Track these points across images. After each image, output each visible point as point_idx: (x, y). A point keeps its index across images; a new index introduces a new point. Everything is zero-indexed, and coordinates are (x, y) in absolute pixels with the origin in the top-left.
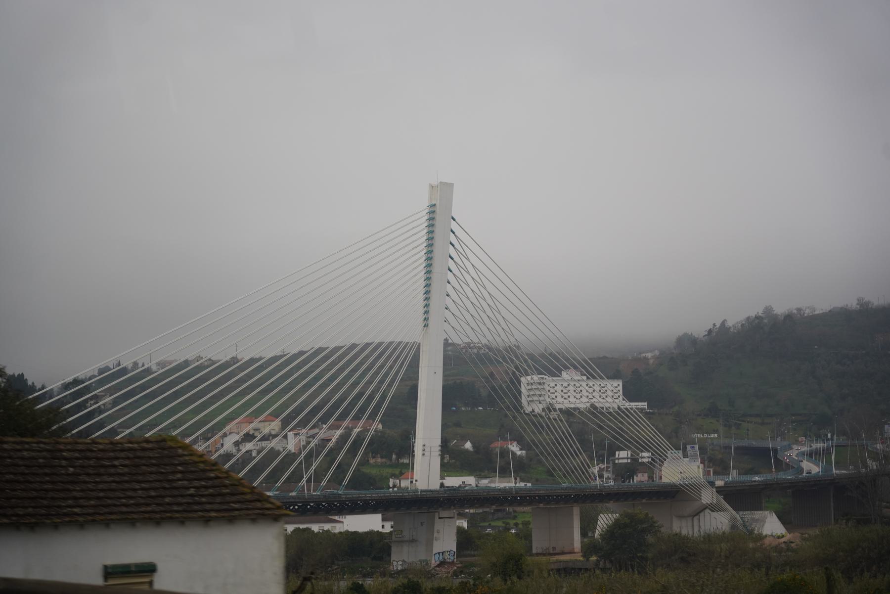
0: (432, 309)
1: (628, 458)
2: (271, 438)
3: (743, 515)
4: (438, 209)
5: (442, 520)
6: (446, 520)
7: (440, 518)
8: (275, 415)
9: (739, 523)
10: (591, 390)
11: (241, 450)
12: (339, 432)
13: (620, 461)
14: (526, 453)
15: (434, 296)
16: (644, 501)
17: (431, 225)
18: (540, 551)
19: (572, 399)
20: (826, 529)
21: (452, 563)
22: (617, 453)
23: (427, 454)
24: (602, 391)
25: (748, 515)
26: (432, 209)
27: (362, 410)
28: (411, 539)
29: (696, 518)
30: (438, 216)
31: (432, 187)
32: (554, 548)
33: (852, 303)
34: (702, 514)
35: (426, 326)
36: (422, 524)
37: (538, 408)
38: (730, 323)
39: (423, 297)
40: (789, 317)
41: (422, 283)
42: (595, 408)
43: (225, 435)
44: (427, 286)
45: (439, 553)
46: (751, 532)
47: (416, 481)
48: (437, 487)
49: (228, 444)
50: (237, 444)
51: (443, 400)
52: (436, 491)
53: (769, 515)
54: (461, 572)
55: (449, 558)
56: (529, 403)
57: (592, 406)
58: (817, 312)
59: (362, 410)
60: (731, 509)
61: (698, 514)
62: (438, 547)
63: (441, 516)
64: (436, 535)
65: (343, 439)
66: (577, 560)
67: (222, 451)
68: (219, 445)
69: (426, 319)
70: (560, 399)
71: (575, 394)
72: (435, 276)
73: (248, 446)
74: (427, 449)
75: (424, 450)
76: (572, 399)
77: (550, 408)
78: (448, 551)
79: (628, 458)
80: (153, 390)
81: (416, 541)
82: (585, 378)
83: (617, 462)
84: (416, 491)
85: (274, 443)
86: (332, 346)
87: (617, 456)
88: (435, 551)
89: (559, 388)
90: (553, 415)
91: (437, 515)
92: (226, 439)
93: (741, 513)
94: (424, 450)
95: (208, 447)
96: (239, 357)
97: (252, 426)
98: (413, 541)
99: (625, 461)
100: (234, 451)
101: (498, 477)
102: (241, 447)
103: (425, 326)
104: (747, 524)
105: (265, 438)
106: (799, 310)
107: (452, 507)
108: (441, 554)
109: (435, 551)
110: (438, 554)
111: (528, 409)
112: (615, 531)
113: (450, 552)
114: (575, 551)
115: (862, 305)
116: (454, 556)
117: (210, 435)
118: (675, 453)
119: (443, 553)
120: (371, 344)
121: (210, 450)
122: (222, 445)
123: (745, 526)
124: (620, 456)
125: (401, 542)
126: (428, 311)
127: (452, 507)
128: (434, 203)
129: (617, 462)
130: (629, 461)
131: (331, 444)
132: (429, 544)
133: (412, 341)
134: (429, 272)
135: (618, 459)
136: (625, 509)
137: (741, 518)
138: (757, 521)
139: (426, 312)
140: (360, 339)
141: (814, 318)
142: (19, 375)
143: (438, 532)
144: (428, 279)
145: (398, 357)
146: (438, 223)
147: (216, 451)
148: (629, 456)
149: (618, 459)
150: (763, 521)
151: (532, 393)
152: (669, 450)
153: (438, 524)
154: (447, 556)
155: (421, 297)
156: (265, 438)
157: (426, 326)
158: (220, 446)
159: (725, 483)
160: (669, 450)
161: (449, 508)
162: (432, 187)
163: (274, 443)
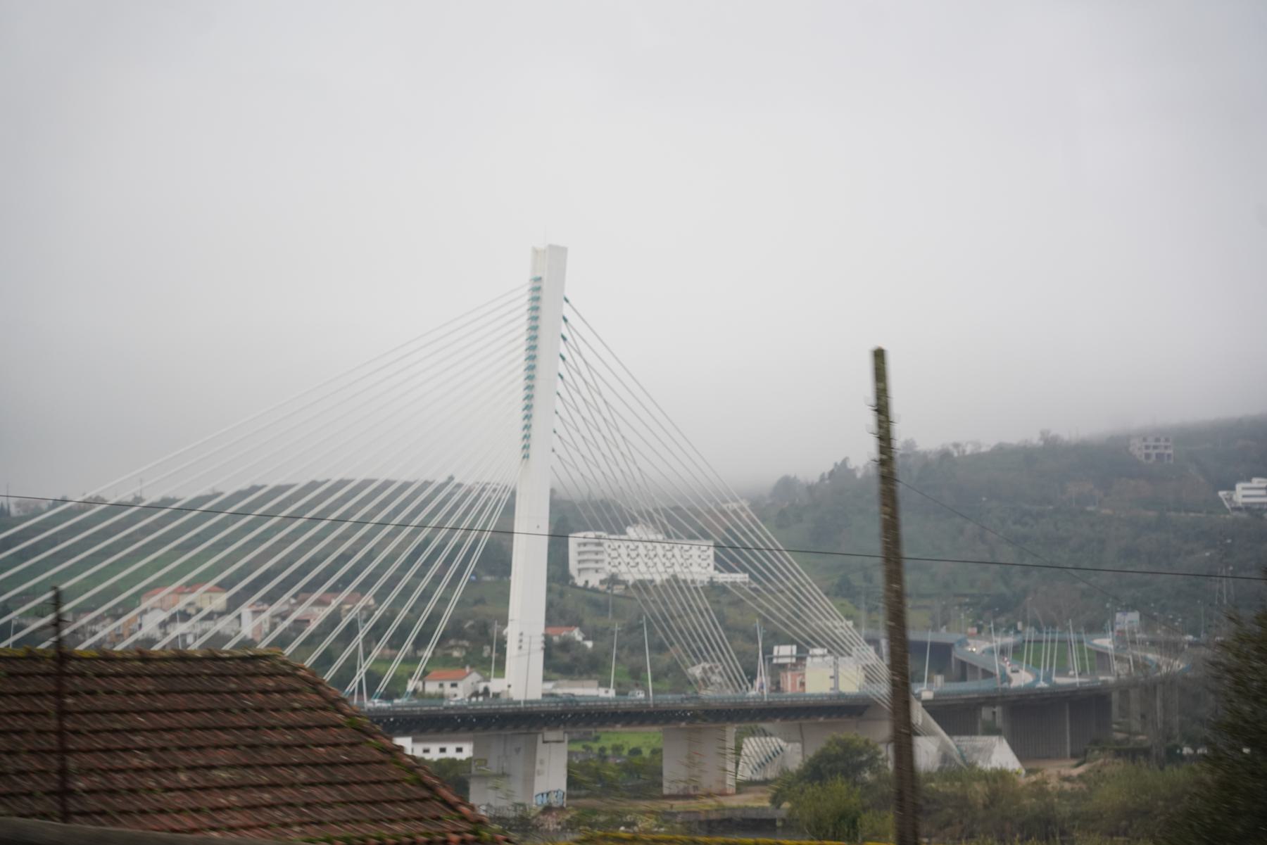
0: (534, 432)
1: (791, 656)
2: (215, 616)
3: (959, 741)
4: (545, 285)
5: (548, 745)
6: (554, 745)
7: (545, 742)
8: (224, 586)
9: (955, 753)
10: (633, 554)
11: (168, 634)
12: (328, 610)
13: (781, 661)
14: (594, 646)
15: (537, 413)
16: (821, 719)
17: (535, 309)
18: (674, 791)
19: (695, 568)
21: (562, 808)
22: (776, 648)
23: (525, 646)
24: (703, 557)
25: (966, 741)
26: (537, 285)
27: (345, 581)
28: (500, 772)
30: (545, 295)
33: (1035, 439)
35: (526, 457)
36: (518, 750)
37: (594, 580)
38: (852, 464)
39: (523, 414)
40: (945, 455)
41: (521, 393)
42: (677, 581)
43: (145, 612)
44: (529, 397)
45: (542, 794)
46: (972, 766)
49: (150, 626)
50: (163, 625)
51: (549, 564)
52: (537, 702)
53: (997, 742)
54: (579, 823)
55: (555, 801)
56: (580, 570)
57: (675, 577)
58: (984, 449)
59: (345, 581)
60: (938, 729)
62: (541, 785)
63: (546, 739)
64: (538, 767)
65: (333, 620)
66: (746, 807)
67: (139, 635)
68: (135, 626)
69: (526, 447)
70: (623, 568)
71: (699, 561)
72: (540, 384)
73: (179, 629)
74: (526, 639)
75: (521, 641)
76: (642, 568)
77: (613, 580)
78: (554, 792)
79: (791, 656)
80: (163, 547)
81: (508, 776)
82: (660, 537)
85: (222, 625)
86: (272, 484)
87: (775, 653)
88: (536, 792)
89: (623, 551)
90: (618, 589)
91: (540, 738)
92: (147, 618)
93: (956, 738)
94: (521, 641)
96: (144, 496)
97: (190, 598)
98: (504, 775)
100: (158, 634)
101: (495, 670)
102: (169, 629)
103: (524, 457)
104: (965, 755)
105: (210, 617)
106: (956, 446)
107: (562, 726)
108: (545, 796)
109: (536, 792)
110: (541, 796)
111: (580, 582)
112: (822, 766)
113: (557, 792)
114: (728, 792)
115: (1046, 441)
116: (563, 798)
117: (120, 611)
118: (863, 650)
119: (548, 794)
120: (348, 482)
121: (121, 632)
122: (140, 626)
123: (963, 757)
124: (781, 653)
125: (484, 777)
126: (530, 436)
127: (562, 726)
128: (538, 275)
129: (775, 661)
130: (794, 660)
131: (313, 626)
132: (529, 780)
133: (468, 482)
134: (530, 378)
135: (778, 657)
137: (957, 746)
138: (980, 750)
139: (526, 437)
140: (329, 472)
141: (978, 458)
143: (542, 762)
144: (529, 387)
145: (471, 506)
146: (545, 305)
147: (130, 635)
148: (794, 652)
149: (778, 657)
150: (988, 751)
151: (585, 557)
152: (853, 645)
153: (542, 751)
154: (553, 798)
156: (210, 617)
157: (526, 457)
158: (137, 627)
159: (935, 695)
160: (853, 645)
161: (557, 727)
163: (222, 625)
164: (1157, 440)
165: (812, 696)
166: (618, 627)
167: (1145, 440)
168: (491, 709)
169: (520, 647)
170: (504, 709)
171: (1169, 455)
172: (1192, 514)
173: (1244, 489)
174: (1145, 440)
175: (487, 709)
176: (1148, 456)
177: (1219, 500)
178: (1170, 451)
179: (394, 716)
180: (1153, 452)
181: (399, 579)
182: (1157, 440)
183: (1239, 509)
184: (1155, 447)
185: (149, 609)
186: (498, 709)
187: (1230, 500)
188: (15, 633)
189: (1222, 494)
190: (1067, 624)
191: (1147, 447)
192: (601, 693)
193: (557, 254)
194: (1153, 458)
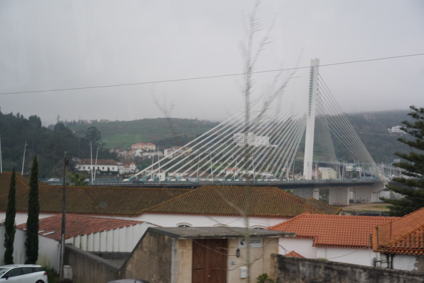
1: (351, 169)
13: (348, 170)
20: (96, 168)
29: (379, 193)
31: (312, 60)
32: (338, 203)
34: (380, 193)
36: (307, 193)
47: (305, 176)
48: (310, 179)
61: (379, 192)
74: (309, 164)
83: (346, 170)
84: (305, 180)
95: (175, 155)
99: (350, 170)
129: (346, 170)
136: (208, 176)
142: (31, 118)
149: (347, 169)
155: (308, 103)
162: (312, 60)
164: (371, 115)
165: (324, 180)
166: (27, 143)
167: (368, 115)
168: (180, 184)
169: (308, 166)
170: (166, 184)
171: (374, 120)
172: (382, 134)
173: (395, 128)
174: (368, 115)
175: (179, 184)
176: (369, 119)
177: (388, 131)
178: (374, 118)
179: (192, 188)
180: (370, 119)
181: (219, 140)
182: (371, 115)
183: (393, 133)
184: (371, 117)
185: (210, 151)
186: (183, 184)
187: (390, 131)
188: (160, 159)
189: (389, 129)
190: (89, 144)
191: (369, 117)
192: (277, 180)
193: (317, 60)
194: (370, 120)
